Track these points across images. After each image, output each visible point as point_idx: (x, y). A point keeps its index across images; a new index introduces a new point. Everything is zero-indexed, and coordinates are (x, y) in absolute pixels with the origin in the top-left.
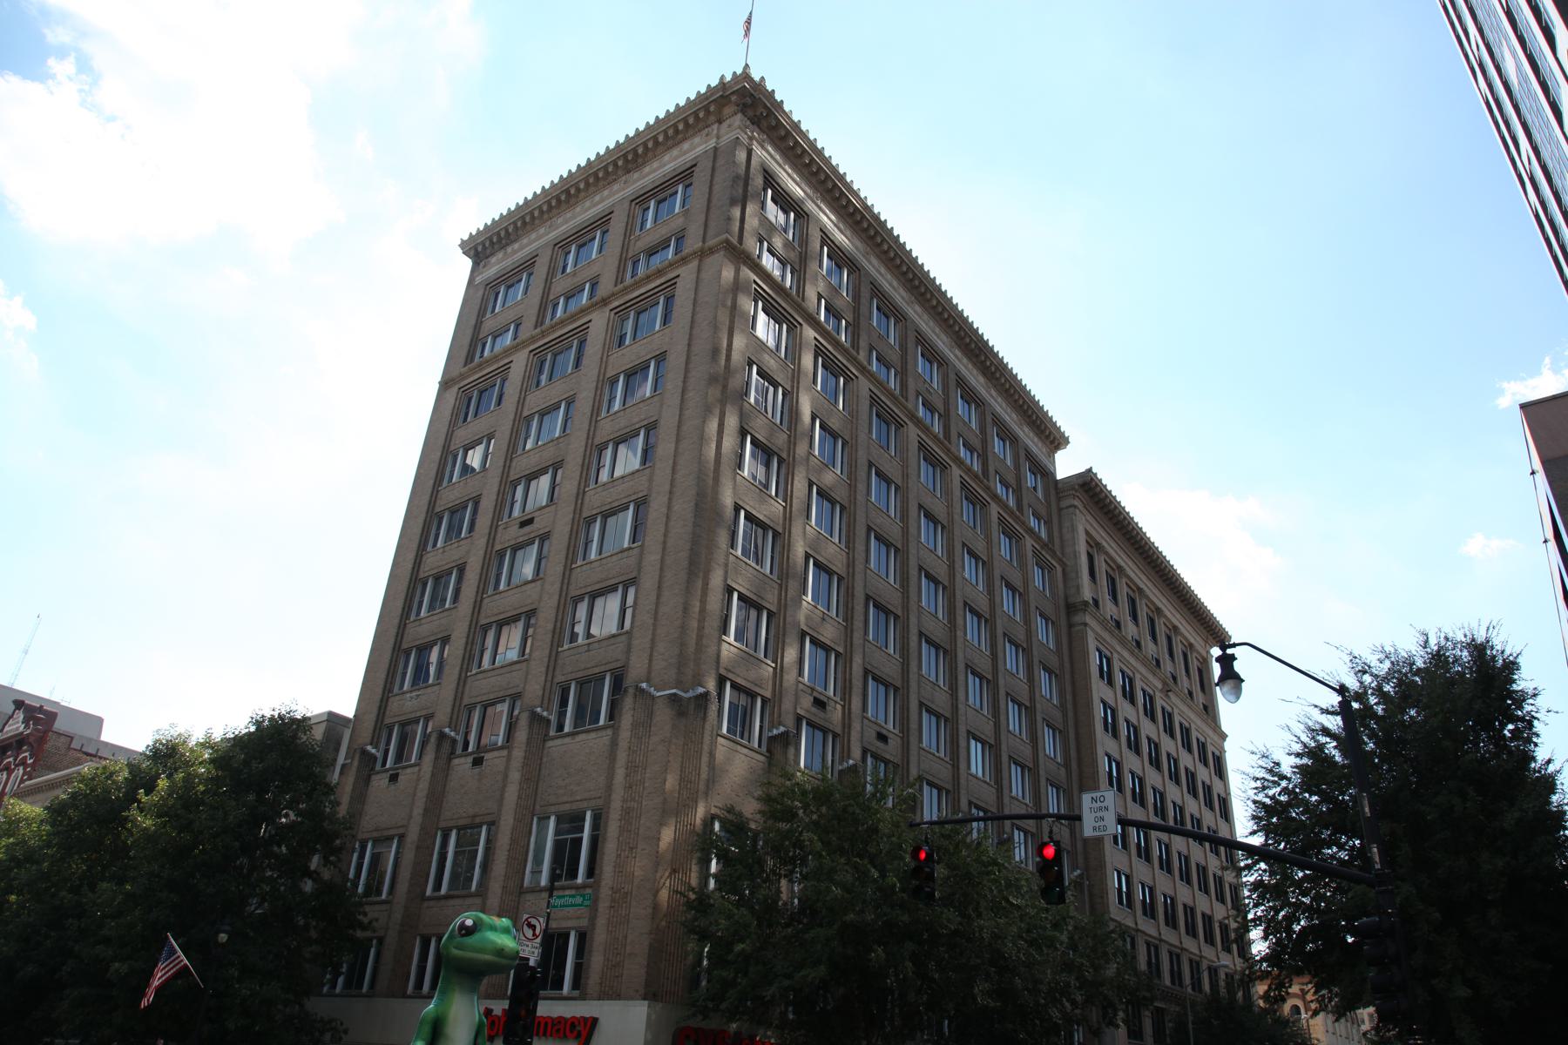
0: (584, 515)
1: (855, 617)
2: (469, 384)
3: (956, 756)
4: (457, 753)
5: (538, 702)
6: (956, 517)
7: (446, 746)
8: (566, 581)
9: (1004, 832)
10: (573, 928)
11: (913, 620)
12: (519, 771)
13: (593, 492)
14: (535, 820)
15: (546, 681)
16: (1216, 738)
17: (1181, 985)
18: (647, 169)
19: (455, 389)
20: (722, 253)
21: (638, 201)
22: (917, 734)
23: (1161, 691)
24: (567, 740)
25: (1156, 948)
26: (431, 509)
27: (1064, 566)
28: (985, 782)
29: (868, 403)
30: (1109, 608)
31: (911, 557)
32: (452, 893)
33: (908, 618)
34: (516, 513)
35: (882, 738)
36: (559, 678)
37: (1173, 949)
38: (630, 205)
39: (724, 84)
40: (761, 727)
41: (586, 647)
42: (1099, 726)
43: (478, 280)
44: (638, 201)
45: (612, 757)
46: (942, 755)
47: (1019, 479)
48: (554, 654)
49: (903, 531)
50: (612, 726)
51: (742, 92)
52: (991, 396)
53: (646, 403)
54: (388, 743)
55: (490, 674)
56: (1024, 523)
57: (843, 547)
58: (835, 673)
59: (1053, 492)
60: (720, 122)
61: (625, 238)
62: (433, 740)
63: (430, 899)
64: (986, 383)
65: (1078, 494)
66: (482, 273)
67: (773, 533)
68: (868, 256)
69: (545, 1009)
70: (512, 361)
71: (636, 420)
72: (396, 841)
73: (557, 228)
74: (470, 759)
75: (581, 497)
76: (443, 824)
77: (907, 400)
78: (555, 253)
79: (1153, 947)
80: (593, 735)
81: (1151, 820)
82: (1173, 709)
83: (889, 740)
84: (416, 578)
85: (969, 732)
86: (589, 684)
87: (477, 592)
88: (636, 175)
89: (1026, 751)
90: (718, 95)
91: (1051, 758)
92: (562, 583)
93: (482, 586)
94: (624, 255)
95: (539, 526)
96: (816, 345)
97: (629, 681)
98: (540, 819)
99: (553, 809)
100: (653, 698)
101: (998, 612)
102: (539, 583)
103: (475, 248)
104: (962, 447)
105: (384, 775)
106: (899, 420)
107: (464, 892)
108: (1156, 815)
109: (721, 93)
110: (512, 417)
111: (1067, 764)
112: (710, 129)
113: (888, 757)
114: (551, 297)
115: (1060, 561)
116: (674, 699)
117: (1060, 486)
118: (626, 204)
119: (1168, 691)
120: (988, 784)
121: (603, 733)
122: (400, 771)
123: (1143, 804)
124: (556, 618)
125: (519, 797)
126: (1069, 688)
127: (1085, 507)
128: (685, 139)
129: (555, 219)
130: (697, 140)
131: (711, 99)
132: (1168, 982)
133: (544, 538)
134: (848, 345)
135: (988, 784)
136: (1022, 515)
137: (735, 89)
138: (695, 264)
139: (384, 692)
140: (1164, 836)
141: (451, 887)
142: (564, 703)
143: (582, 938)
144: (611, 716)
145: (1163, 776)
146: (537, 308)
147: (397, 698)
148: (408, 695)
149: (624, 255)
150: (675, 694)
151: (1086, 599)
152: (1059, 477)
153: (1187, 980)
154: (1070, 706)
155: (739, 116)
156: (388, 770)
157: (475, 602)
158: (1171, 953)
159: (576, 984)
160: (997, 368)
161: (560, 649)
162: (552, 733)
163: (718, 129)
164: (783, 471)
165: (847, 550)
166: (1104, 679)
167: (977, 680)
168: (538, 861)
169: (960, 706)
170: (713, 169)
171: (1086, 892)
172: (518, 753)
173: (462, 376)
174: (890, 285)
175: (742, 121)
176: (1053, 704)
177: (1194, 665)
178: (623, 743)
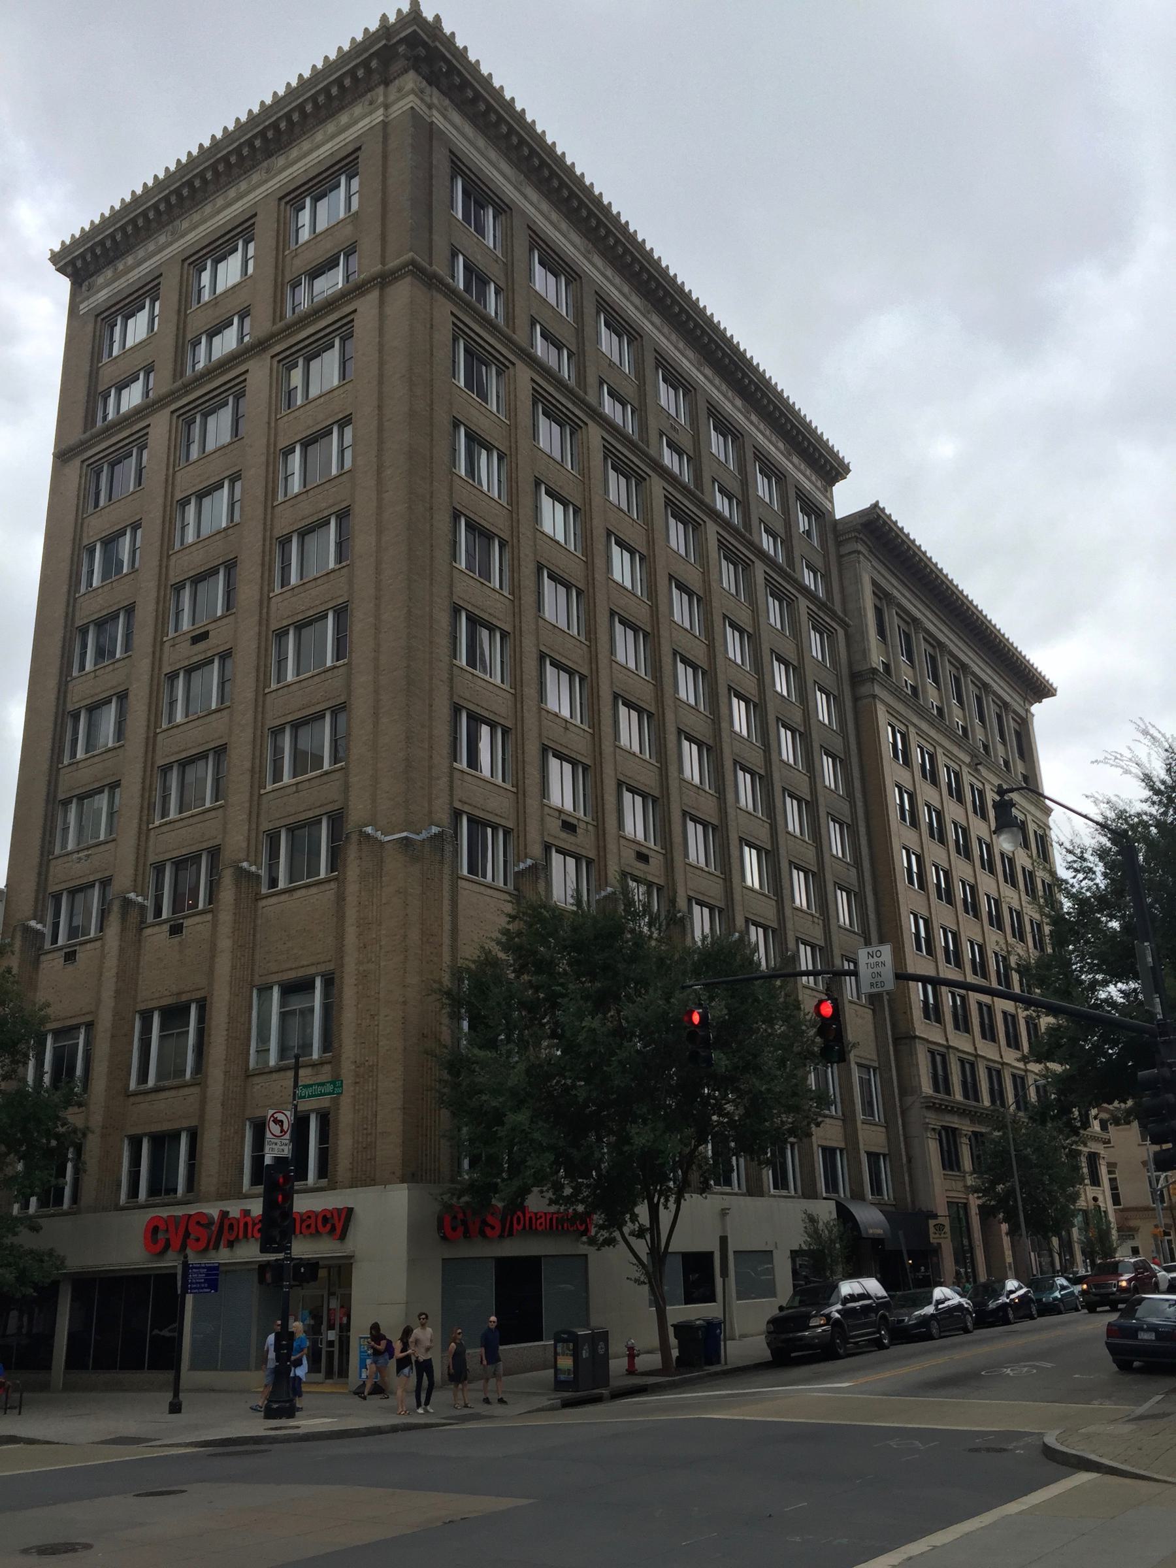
0: (273, 627)
1: (603, 722)
2: (99, 453)
3: (728, 867)
4: (148, 921)
5: (242, 855)
6: (714, 585)
7: (134, 914)
8: (260, 709)
9: (787, 950)
10: (312, 1111)
11: (670, 716)
12: (229, 937)
13: (279, 598)
14: (255, 992)
15: (249, 830)
16: (1038, 814)
17: (1003, 1104)
18: (294, 153)
19: (77, 462)
20: (408, 279)
21: (288, 198)
22: (681, 848)
23: (969, 765)
24: (283, 898)
25: (972, 1065)
26: (69, 623)
27: (845, 626)
28: (763, 894)
29: (601, 455)
30: (906, 674)
31: (663, 641)
32: (161, 1084)
33: (664, 714)
34: (186, 625)
35: (643, 857)
36: (266, 826)
37: (991, 1064)
38: (279, 205)
39: (388, 29)
40: (505, 862)
41: (294, 788)
42: (894, 815)
43: (83, 308)
44: (288, 198)
45: (340, 915)
46: (712, 870)
47: (789, 524)
48: (256, 798)
49: (652, 611)
50: (336, 879)
51: (412, 41)
52: (752, 423)
53: (334, 483)
54: (57, 914)
55: (178, 825)
56: (796, 581)
57: (583, 640)
58: (584, 790)
59: (830, 536)
60: (387, 83)
61: (277, 254)
62: (116, 908)
63: (136, 1094)
64: (744, 406)
65: (861, 536)
66: (88, 298)
67: (501, 634)
68: (590, 256)
69: (302, 1204)
70: (149, 425)
71: (324, 505)
72: (83, 1031)
73: (182, 236)
74: (166, 927)
75: (265, 604)
76: (142, 1007)
77: (648, 447)
78: (185, 272)
79: (969, 1065)
80: (314, 890)
81: (969, 980)
82: (983, 784)
83: (651, 860)
84: (64, 711)
85: (741, 839)
86: (302, 829)
87: (148, 727)
88: (281, 161)
89: (810, 854)
90: (380, 45)
91: (839, 858)
92: (256, 712)
93: (152, 719)
94: (280, 280)
95: (216, 642)
96: (533, 388)
97: (351, 823)
98: (260, 990)
99: (275, 978)
100: (382, 844)
101: (769, 693)
102: (225, 713)
103: (72, 263)
104: (717, 493)
105: (56, 955)
106: (640, 472)
107: (176, 1082)
108: (975, 973)
109: (384, 42)
110: (160, 500)
111: (857, 863)
112: (373, 93)
113: (650, 878)
114: (189, 337)
115: (845, 626)
116: (406, 843)
117: (839, 527)
118: (273, 204)
119: (977, 764)
120: (766, 896)
121: (327, 887)
122: (77, 948)
123: (959, 964)
124: (254, 755)
125: (234, 967)
126: (856, 774)
127: (871, 551)
128: (341, 109)
129: (177, 222)
130: (358, 110)
131: (372, 51)
132: (987, 1103)
133: (225, 656)
134: (572, 383)
135: (766, 896)
136: (794, 571)
137: (403, 35)
138: (374, 295)
139: (42, 854)
140: (986, 999)
141: (160, 1076)
142: (274, 855)
143: (325, 1120)
144: (333, 866)
145: (974, 866)
146: (172, 350)
147: (60, 861)
148: (75, 856)
149: (280, 280)
150: (406, 838)
151: (874, 665)
152: (838, 516)
153: (1010, 1098)
154: (858, 795)
155: (412, 75)
156: (60, 949)
157: (147, 738)
158: (989, 1069)
159: (323, 1172)
160: (758, 388)
161: (262, 792)
162: (264, 890)
163: (386, 96)
164: (507, 556)
165: (587, 643)
166: (898, 760)
167: (690, 670)
168: (264, 1038)
169: (729, 810)
170: (385, 157)
171: (887, 1009)
172: (226, 917)
173: (83, 446)
174: (620, 292)
175: (415, 82)
176: (839, 795)
177: (1011, 725)
178: (351, 900)
